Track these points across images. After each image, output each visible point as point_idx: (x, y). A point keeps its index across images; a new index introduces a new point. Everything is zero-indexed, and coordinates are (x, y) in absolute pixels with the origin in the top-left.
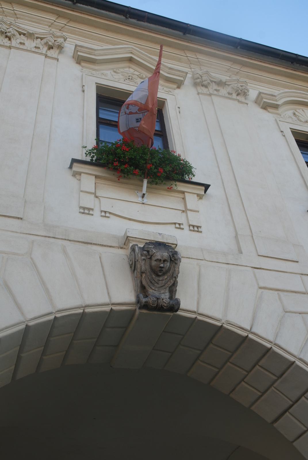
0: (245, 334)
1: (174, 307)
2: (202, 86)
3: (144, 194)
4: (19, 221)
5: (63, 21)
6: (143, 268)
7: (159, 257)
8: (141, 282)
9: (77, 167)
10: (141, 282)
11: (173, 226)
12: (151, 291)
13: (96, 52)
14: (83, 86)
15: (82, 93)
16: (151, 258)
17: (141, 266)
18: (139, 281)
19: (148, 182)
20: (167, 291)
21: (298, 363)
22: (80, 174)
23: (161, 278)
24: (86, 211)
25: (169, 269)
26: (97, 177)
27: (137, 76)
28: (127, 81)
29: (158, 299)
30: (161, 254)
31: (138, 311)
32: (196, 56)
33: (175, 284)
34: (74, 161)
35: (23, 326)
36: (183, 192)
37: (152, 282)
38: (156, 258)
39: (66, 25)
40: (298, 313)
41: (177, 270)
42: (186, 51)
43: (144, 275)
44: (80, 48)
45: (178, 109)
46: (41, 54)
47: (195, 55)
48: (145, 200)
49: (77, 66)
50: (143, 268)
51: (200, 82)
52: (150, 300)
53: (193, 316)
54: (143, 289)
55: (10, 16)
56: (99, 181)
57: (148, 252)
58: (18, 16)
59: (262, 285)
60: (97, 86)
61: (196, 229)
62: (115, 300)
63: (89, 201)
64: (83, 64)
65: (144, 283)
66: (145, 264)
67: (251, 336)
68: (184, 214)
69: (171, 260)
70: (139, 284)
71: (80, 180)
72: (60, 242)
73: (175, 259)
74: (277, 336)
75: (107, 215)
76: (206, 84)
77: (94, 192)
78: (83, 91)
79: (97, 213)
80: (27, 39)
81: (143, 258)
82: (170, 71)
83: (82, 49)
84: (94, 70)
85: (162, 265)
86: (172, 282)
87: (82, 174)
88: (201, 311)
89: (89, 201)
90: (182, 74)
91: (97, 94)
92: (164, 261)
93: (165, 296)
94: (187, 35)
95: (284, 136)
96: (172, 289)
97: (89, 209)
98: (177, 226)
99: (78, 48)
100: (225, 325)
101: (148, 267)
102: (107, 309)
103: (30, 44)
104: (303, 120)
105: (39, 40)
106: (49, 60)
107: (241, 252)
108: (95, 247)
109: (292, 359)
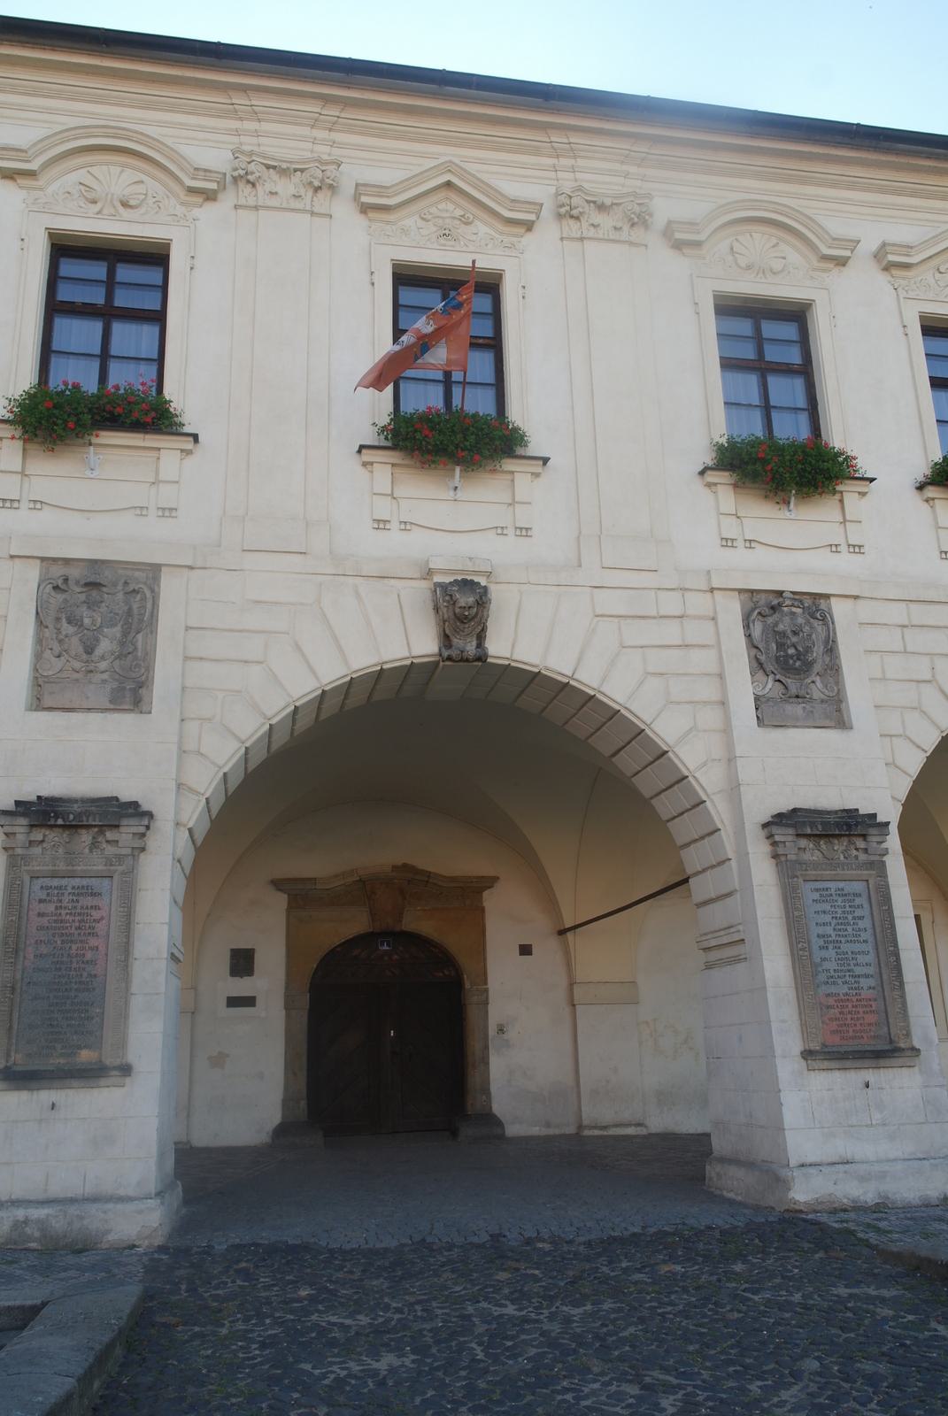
0: (565, 680)
1: (482, 657)
2: (572, 217)
3: (456, 487)
4: (303, 555)
5: (333, 111)
6: (446, 616)
7: (463, 605)
8: (444, 631)
9: (368, 456)
10: (444, 631)
11: (494, 530)
12: (455, 641)
13: (390, 191)
14: (372, 273)
15: (370, 286)
16: (454, 604)
17: (443, 614)
18: (442, 629)
19: (461, 471)
20: (474, 639)
21: (623, 711)
22: (372, 464)
23: (467, 626)
24: (381, 524)
25: (477, 614)
26: (393, 465)
27: (458, 222)
28: (442, 241)
29: (462, 652)
30: (466, 600)
31: (441, 663)
32: (568, 138)
33: (484, 630)
34: (362, 447)
35: (320, 691)
36: (512, 472)
37: (456, 631)
38: (460, 605)
39: (338, 117)
40: (917, 264)
41: (485, 613)
42: (549, 131)
43: (447, 624)
44: (363, 188)
45: (521, 291)
46: (304, 211)
47: (566, 135)
48: (460, 494)
49: (363, 216)
50: (446, 616)
51: (567, 211)
52: (454, 653)
53: (507, 662)
54: (446, 640)
55: (247, 119)
56: (397, 470)
57: (451, 596)
58: (261, 116)
59: (599, 612)
60: (394, 264)
61: (524, 533)
62: (415, 653)
63: (384, 509)
64: (370, 215)
65: (447, 632)
66: (447, 611)
67: (572, 683)
68: (511, 508)
69: (478, 603)
70: (442, 634)
71: (372, 472)
72: (350, 580)
73: (483, 603)
74: (603, 680)
75: (408, 527)
76: (503, 461)
77: (390, 492)
78: (373, 284)
79: (394, 525)
80: (280, 177)
81: (445, 604)
82: (513, 204)
83: (368, 189)
84: (388, 222)
85: (467, 613)
86: (480, 628)
87: (375, 465)
88: (515, 657)
89: (384, 509)
90: (533, 206)
91: (394, 273)
92: (470, 607)
93: (471, 648)
94: (552, 102)
95: (698, 313)
96: (481, 638)
97: (385, 522)
98: (499, 531)
99: (360, 188)
100: (543, 672)
101: (451, 614)
102: (408, 662)
103: (286, 187)
104: (743, 265)
105: (299, 173)
106: (317, 220)
107: (580, 566)
108: (392, 581)
109: (617, 707)
